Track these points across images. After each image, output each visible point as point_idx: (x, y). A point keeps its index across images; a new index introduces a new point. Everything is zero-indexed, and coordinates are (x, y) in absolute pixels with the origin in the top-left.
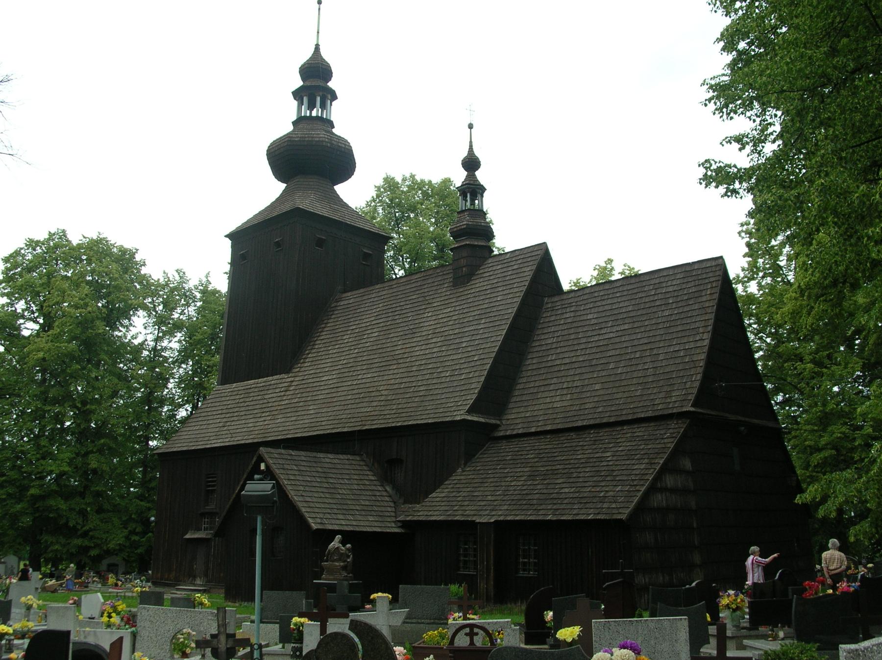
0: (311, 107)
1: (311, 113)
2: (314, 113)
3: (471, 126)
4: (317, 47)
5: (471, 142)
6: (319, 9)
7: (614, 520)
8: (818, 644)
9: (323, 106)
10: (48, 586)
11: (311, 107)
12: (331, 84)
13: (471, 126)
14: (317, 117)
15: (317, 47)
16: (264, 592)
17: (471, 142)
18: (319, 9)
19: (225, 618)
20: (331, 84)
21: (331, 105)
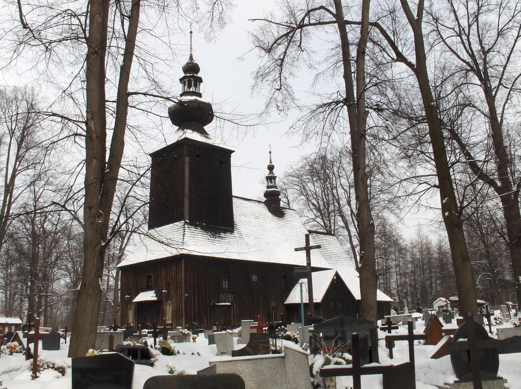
0: (190, 86)
1: (189, 90)
2: (191, 90)
3: (270, 153)
4: (191, 58)
5: (270, 159)
6: (191, 36)
7: (190, 195)
8: (313, 324)
9: (196, 86)
10: (363, 368)
11: (190, 86)
12: (199, 75)
13: (270, 153)
14: (193, 92)
15: (191, 58)
16: (407, 360)
17: (270, 159)
18: (191, 36)
19: (58, 115)
20: (199, 75)
21: (200, 85)
